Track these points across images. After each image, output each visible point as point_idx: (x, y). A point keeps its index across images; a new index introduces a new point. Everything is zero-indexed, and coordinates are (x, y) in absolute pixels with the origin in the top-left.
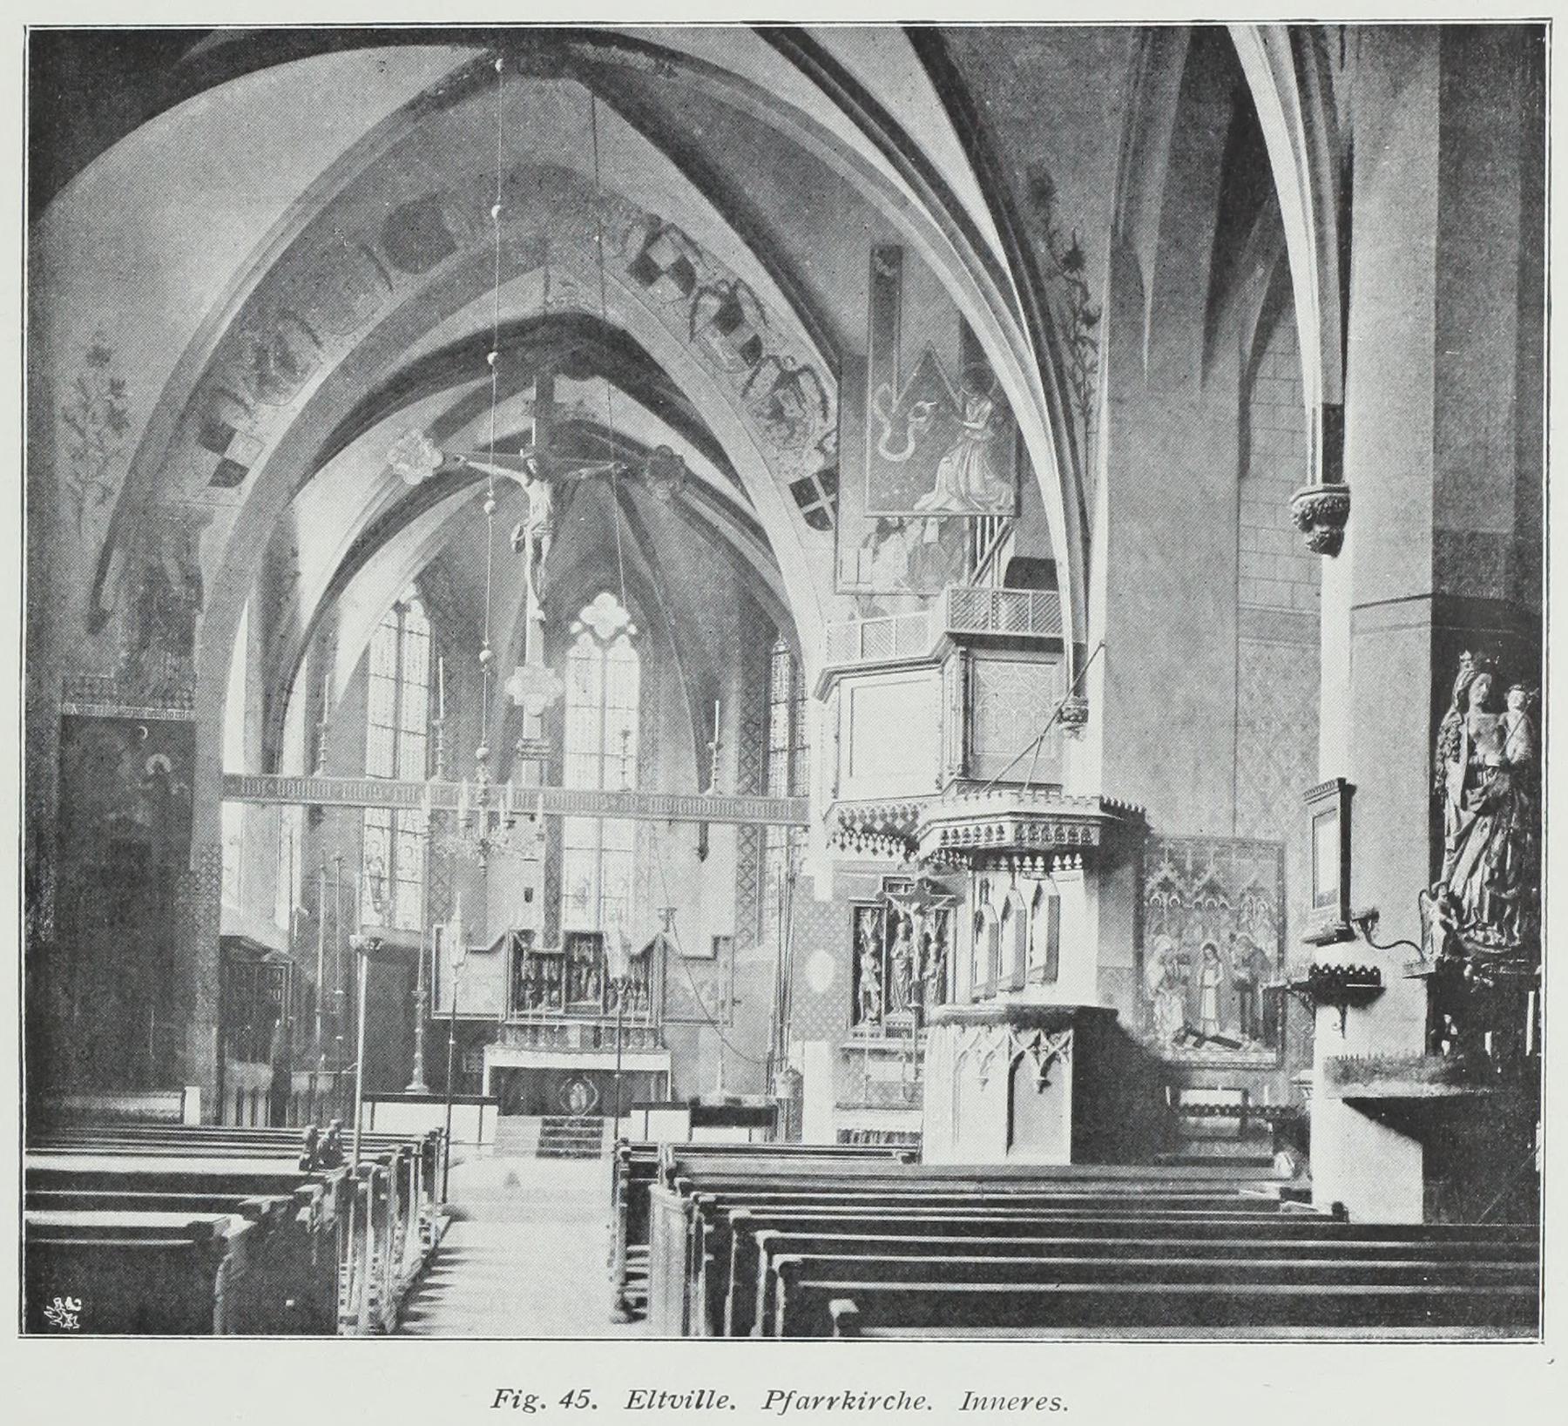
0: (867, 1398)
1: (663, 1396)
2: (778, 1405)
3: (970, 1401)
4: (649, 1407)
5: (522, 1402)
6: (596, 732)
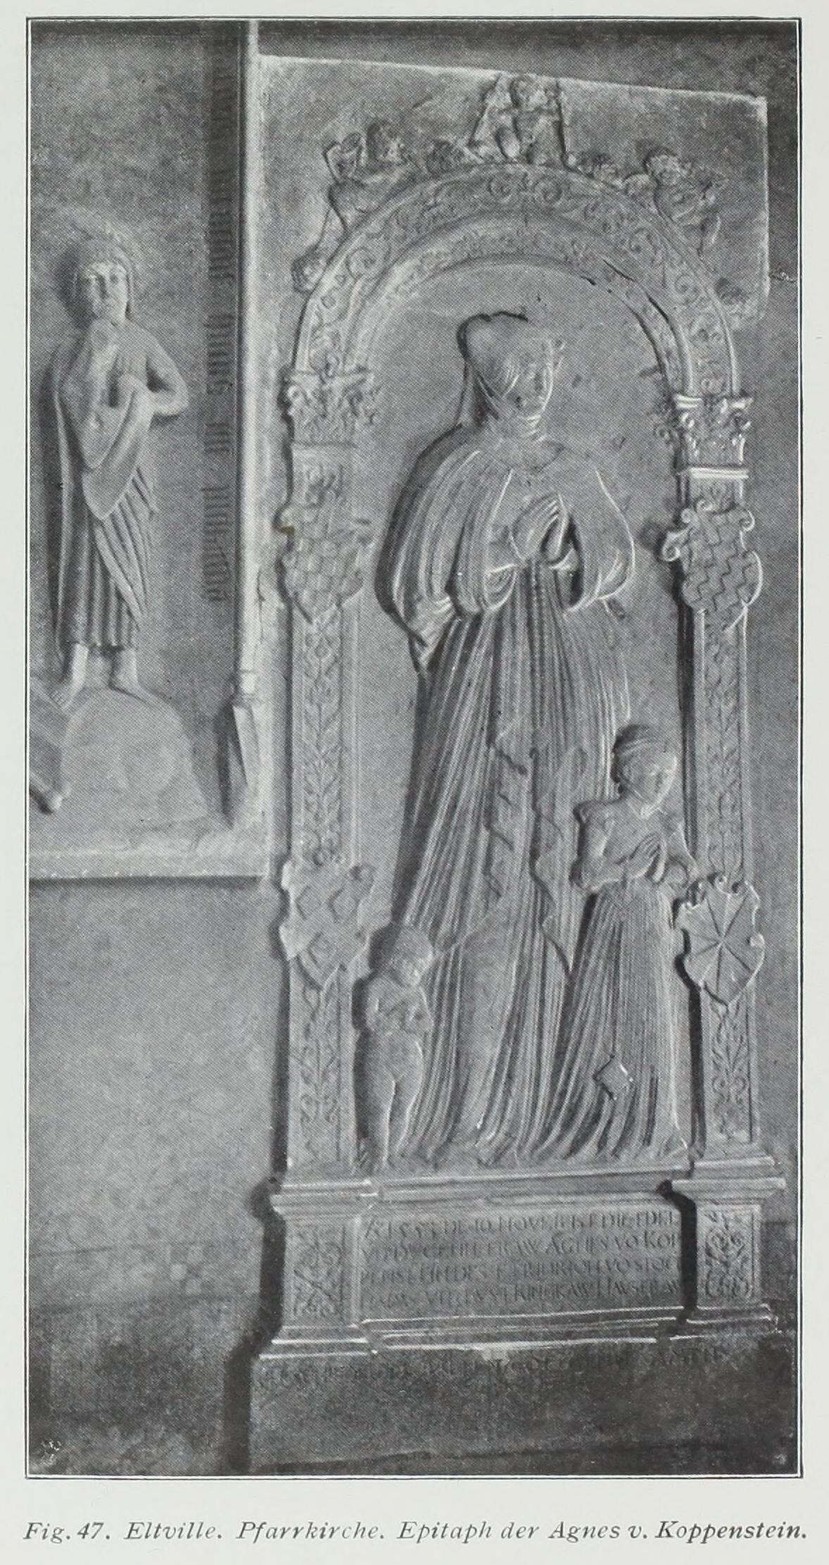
0: (327, 1528)
1: (159, 1527)
2: (250, 1534)
3: (664, 1531)
4: (147, 1537)
5: (50, 1534)
6: (176, 903)
